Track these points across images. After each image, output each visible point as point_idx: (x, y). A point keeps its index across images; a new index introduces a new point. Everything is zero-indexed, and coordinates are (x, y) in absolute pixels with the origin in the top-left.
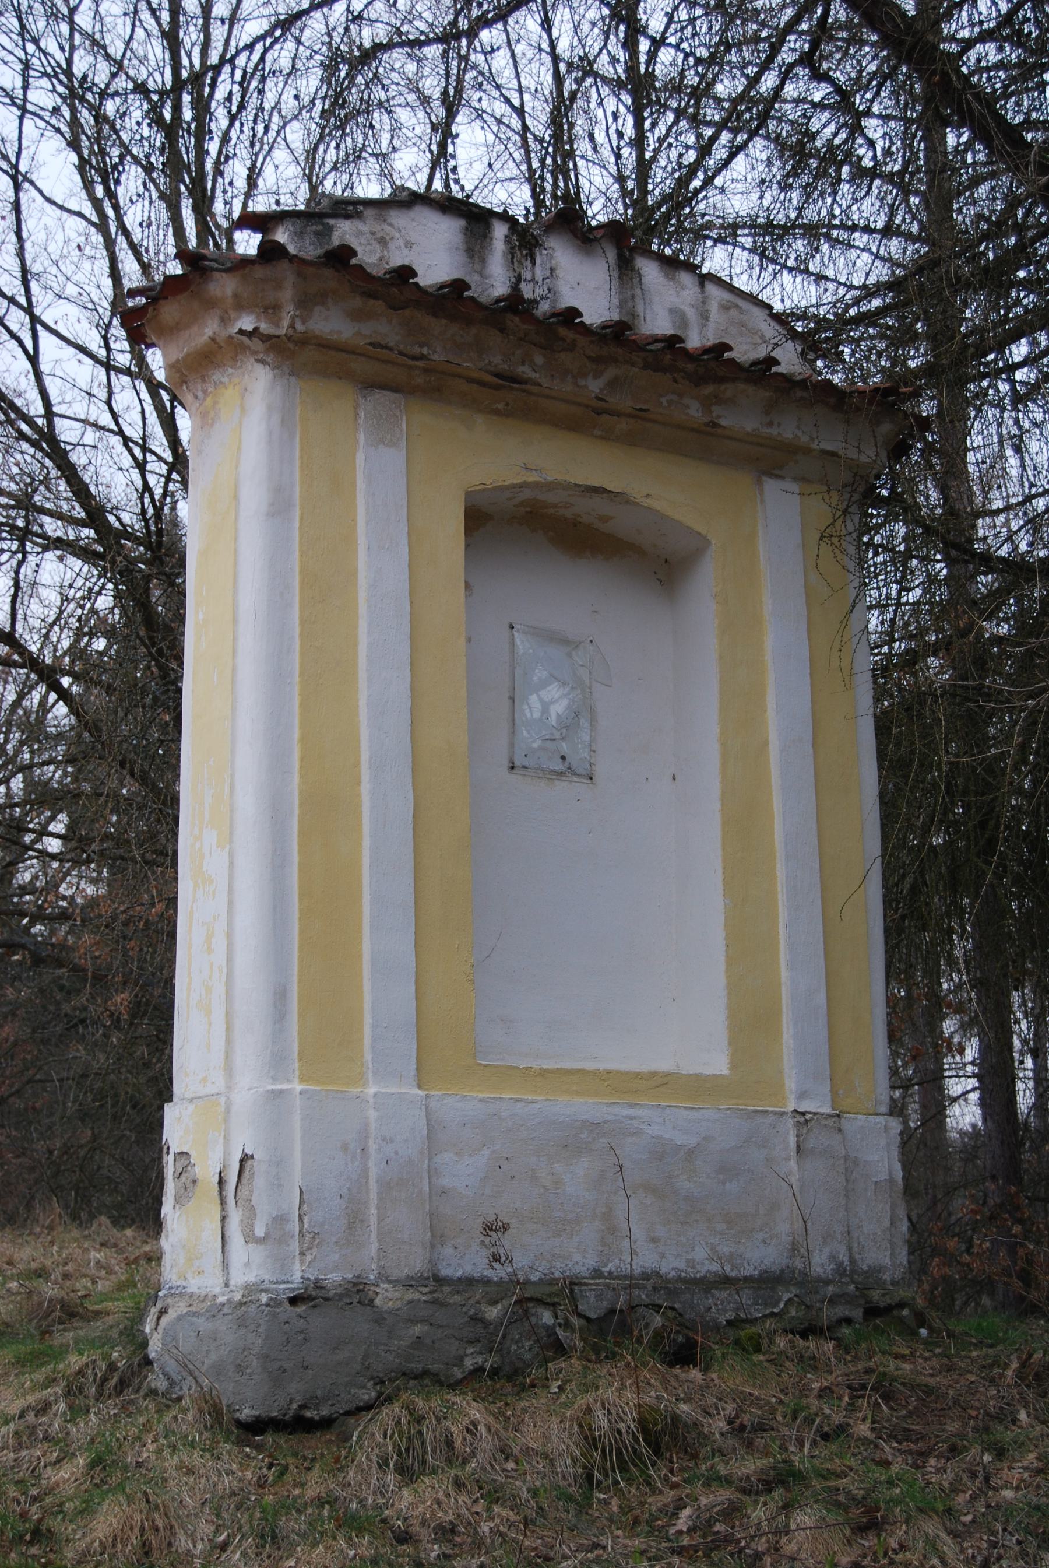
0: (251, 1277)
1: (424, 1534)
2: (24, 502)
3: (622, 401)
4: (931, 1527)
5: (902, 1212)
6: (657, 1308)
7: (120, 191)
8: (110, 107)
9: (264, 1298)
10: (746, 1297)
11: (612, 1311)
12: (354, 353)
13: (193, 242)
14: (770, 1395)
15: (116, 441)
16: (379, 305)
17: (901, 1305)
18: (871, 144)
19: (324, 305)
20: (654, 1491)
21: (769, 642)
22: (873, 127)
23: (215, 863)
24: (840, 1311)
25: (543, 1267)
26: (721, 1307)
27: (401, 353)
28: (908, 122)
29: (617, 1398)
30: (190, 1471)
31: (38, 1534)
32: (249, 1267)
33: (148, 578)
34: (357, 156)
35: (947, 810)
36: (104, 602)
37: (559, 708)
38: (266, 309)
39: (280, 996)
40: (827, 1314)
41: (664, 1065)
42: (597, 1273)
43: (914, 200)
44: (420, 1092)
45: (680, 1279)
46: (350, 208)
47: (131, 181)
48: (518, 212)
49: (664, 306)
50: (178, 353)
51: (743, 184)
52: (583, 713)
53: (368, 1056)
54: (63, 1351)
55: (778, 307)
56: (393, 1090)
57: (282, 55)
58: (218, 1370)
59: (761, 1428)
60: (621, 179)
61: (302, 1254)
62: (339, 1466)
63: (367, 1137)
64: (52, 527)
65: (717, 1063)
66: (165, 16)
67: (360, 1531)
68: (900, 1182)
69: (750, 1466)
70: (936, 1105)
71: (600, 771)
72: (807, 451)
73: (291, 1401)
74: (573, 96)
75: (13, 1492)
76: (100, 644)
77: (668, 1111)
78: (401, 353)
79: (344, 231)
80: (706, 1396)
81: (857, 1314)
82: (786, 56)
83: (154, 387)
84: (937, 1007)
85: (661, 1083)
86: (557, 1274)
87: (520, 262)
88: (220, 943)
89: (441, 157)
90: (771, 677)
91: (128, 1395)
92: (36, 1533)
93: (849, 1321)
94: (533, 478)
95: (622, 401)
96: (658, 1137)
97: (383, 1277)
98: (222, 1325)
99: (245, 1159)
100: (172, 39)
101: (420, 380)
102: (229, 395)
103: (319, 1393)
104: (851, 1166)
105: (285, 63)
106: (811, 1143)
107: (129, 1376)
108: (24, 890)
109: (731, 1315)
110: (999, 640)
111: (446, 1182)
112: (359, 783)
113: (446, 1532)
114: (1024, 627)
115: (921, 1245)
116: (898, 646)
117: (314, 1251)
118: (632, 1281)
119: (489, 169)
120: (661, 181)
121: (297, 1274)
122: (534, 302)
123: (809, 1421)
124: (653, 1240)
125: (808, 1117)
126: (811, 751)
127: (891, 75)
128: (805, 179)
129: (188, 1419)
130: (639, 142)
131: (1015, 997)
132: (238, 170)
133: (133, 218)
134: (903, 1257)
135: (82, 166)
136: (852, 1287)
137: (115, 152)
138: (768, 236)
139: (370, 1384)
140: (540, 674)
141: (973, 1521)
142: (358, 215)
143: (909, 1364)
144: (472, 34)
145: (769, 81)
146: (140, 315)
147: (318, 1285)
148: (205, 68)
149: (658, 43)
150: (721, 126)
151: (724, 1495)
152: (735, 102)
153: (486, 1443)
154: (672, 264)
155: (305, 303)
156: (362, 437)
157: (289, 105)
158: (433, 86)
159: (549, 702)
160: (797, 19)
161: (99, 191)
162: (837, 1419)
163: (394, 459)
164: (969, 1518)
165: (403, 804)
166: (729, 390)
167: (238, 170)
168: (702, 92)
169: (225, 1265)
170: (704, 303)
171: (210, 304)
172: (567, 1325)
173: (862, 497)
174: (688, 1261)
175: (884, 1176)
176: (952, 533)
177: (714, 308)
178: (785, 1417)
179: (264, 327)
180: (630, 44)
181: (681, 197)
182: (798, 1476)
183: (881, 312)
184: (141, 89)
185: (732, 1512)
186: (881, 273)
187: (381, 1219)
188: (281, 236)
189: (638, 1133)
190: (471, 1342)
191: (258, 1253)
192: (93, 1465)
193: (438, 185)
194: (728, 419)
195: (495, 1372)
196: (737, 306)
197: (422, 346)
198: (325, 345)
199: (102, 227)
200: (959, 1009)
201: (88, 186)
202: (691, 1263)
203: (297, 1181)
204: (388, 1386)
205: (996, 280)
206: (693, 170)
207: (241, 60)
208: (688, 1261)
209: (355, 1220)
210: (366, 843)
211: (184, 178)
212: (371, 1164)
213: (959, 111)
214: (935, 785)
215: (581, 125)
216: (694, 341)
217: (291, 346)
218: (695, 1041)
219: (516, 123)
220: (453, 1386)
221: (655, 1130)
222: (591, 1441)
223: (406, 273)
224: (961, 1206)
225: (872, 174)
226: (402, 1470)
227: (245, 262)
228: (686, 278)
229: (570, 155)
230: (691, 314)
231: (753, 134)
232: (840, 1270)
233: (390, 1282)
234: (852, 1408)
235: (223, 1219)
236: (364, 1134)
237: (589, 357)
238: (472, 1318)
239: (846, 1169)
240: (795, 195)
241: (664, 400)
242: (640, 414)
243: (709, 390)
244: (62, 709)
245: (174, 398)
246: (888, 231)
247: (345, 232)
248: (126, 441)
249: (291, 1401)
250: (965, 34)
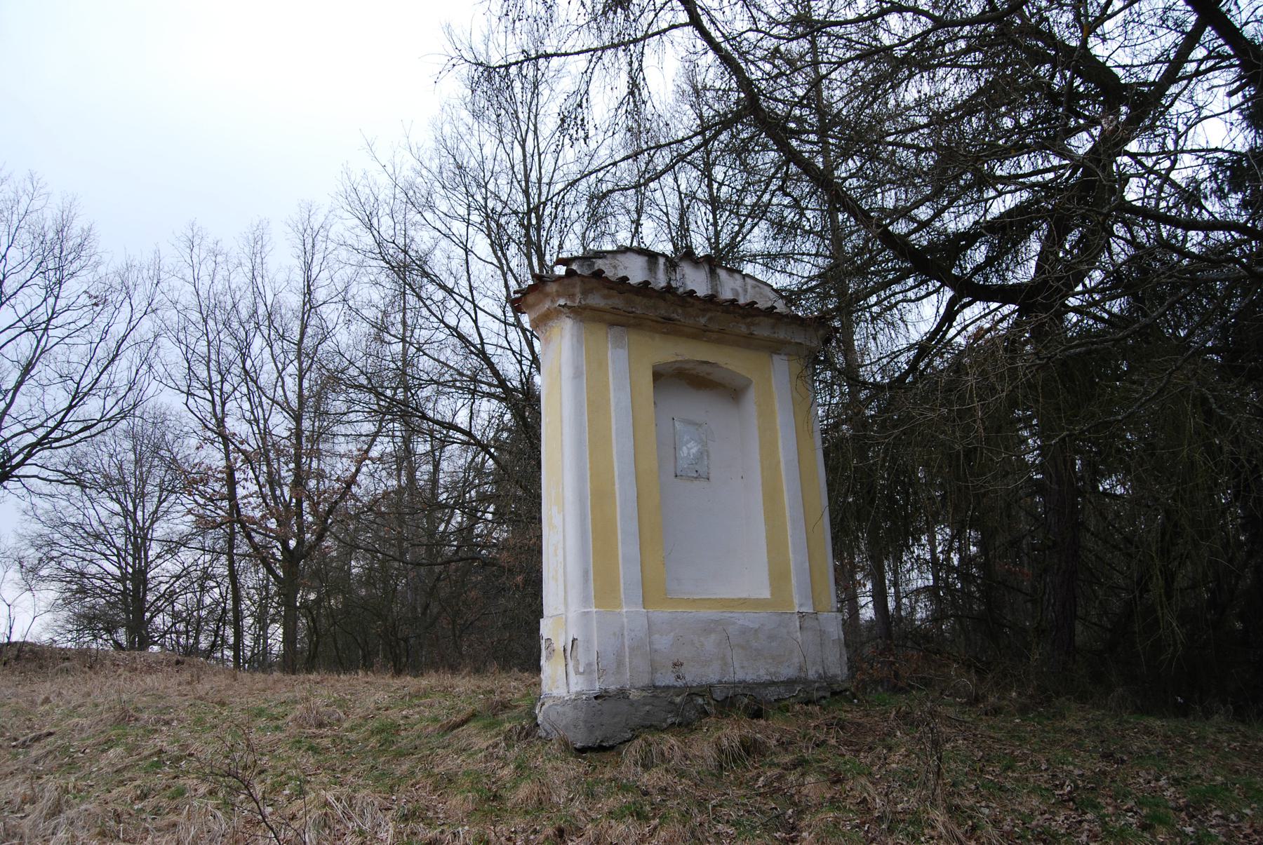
0: (578, 689)
1: (654, 792)
2: (474, 379)
3: (715, 327)
4: (863, 780)
5: (844, 652)
6: (745, 695)
7: (508, 253)
8: (503, 221)
10: (782, 689)
13: (537, 271)
14: (794, 729)
15: (509, 352)
16: (614, 293)
17: (846, 690)
18: (808, 220)
19: (596, 294)
20: (748, 770)
21: (778, 420)
22: (809, 214)
23: (557, 520)
24: (821, 693)
25: (698, 680)
26: (771, 694)
28: (822, 211)
29: (731, 732)
30: (557, 769)
31: (496, 797)
32: (577, 684)
33: (524, 407)
34: (603, 233)
35: (854, 486)
36: (508, 417)
37: (694, 450)
39: (586, 573)
40: (816, 695)
41: (744, 595)
42: (720, 682)
43: (827, 242)
46: (601, 254)
47: (513, 250)
48: (668, 253)
49: (729, 288)
50: (534, 315)
51: (758, 239)
52: (703, 454)
54: (503, 722)
55: (775, 287)
57: (570, 197)
58: (566, 728)
59: (791, 743)
60: (709, 239)
62: (618, 765)
64: (485, 388)
65: (766, 594)
66: (523, 184)
67: (628, 791)
69: (787, 759)
70: (855, 609)
72: (790, 343)
74: (688, 207)
75: (485, 780)
76: (505, 435)
79: (600, 264)
80: (767, 731)
81: (828, 694)
82: (772, 187)
83: (524, 330)
84: (854, 568)
85: (744, 602)
88: (560, 552)
89: (636, 233)
90: (780, 435)
91: (530, 739)
92: (495, 796)
93: (824, 698)
95: (715, 327)
97: (632, 687)
98: (567, 709)
100: (526, 193)
101: (632, 321)
102: (556, 331)
105: (572, 200)
106: (805, 625)
107: (529, 732)
108: (478, 536)
110: (872, 416)
111: (656, 647)
113: (663, 790)
114: (881, 411)
115: (853, 665)
116: (831, 421)
118: (735, 685)
119: (655, 237)
120: (725, 239)
122: (677, 288)
123: (810, 739)
127: (814, 193)
128: (782, 235)
129: (555, 747)
130: (715, 224)
131: (886, 563)
132: (555, 242)
133: (513, 265)
134: (846, 670)
135: (492, 244)
137: (505, 238)
138: (769, 259)
140: (686, 438)
142: (604, 257)
143: (850, 714)
144: (646, 184)
145: (766, 197)
146: (517, 303)
147: (606, 691)
148: (540, 203)
149: (721, 184)
150: (748, 216)
151: (777, 771)
152: (753, 206)
153: (678, 753)
154: (732, 271)
155: (585, 293)
157: (574, 215)
158: (632, 206)
159: (690, 449)
160: (776, 172)
161: (500, 254)
162: (822, 738)
163: (623, 354)
166: (757, 320)
167: (555, 242)
168: (739, 204)
169: (568, 684)
171: (547, 295)
172: (709, 704)
173: (813, 360)
176: (850, 375)
177: (749, 288)
179: (569, 303)
180: (710, 186)
181: (733, 245)
182: (807, 762)
183: (816, 286)
184: (516, 213)
185: (780, 778)
186: (815, 271)
188: (574, 267)
189: (734, 623)
191: (581, 679)
192: (517, 768)
193: (635, 244)
194: (757, 332)
195: (680, 724)
198: (593, 309)
199: (501, 268)
200: (863, 569)
201: (495, 252)
204: (637, 731)
205: (862, 272)
206: (737, 234)
207: (555, 199)
209: (620, 664)
210: (618, 509)
211: (533, 247)
213: (843, 205)
214: (848, 477)
215: (691, 219)
216: (742, 301)
218: (753, 583)
219: (665, 219)
220: (663, 731)
221: (740, 622)
222: (721, 751)
223: (625, 279)
224: (868, 650)
225: (810, 232)
226: (643, 766)
227: (560, 277)
228: (737, 276)
229: (688, 230)
230: (740, 290)
231: (761, 219)
232: (820, 676)
234: (828, 733)
236: (623, 627)
240: (779, 242)
242: (721, 331)
243: (749, 320)
244: (491, 462)
245: (532, 334)
246: (817, 255)
248: (514, 352)
250: (844, 175)
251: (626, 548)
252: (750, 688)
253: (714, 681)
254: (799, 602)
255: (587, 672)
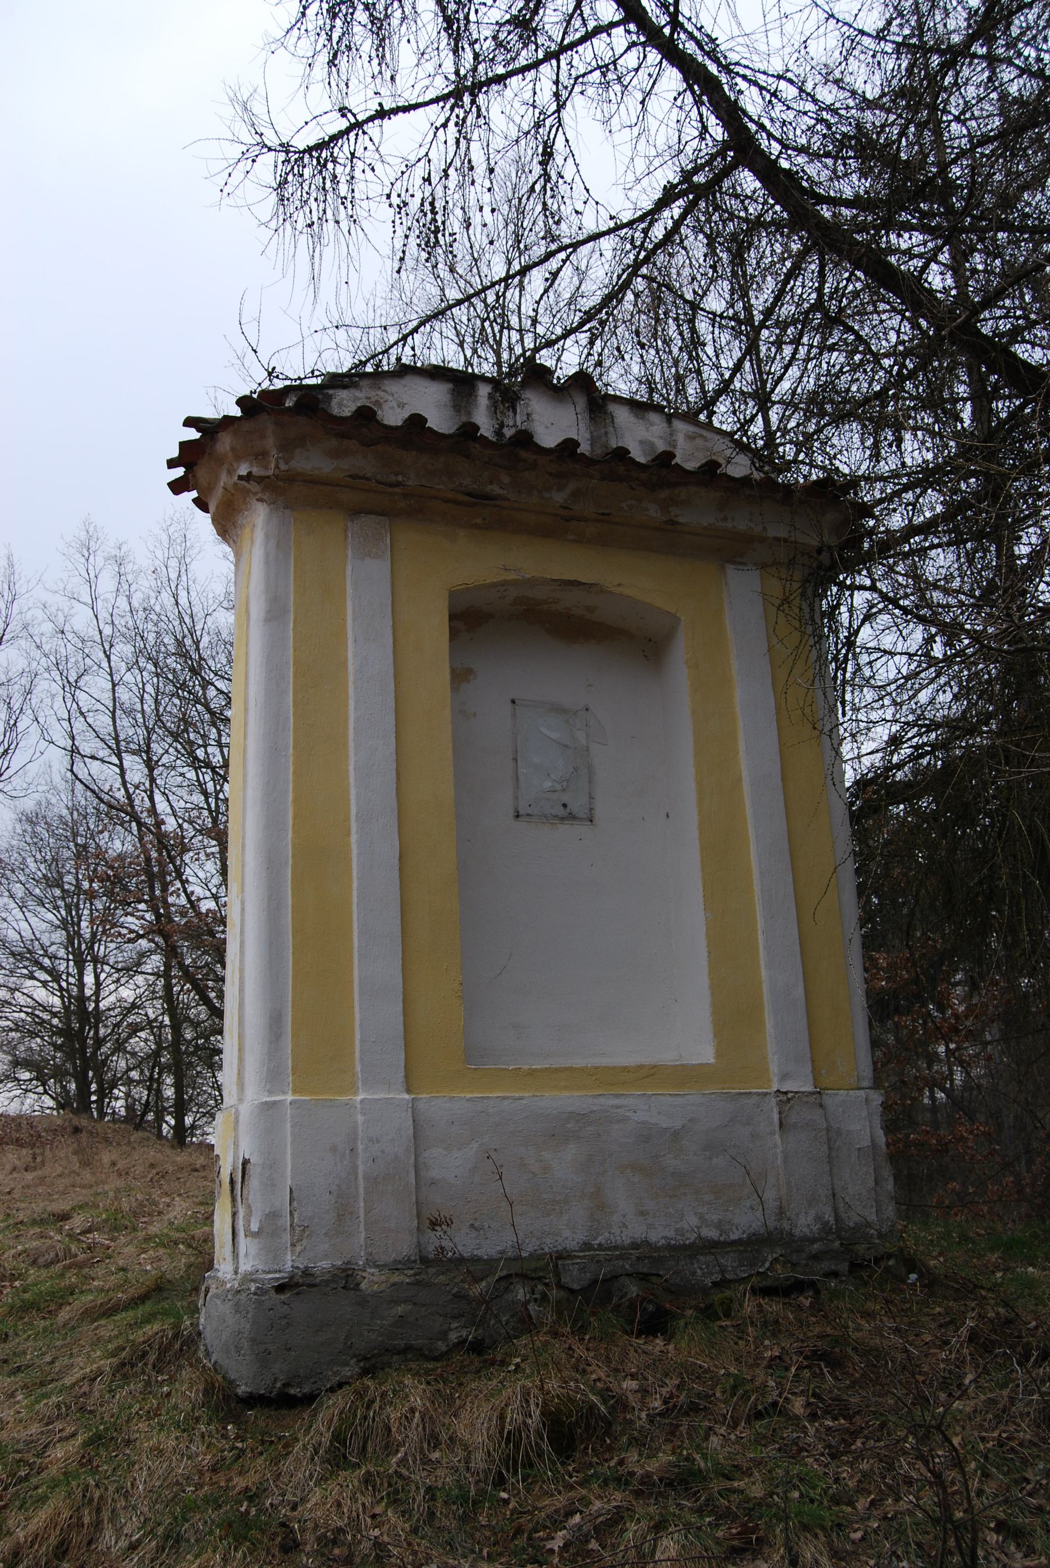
9: (253, 1287)
10: (728, 1261)
11: (596, 1281)
12: (338, 485)
24: (826, 1265)
26: (702, 1271)
27: (378, 482)
38: (256, 456)
39: (275, 1021)
42: (587, 1246)
44: (407, 1096)
45: (669, 1247)
53: (358, 1068)
56: (382, 1096)
61: (293, 1245)
63: (355, 1139)
65: (705, 1053)
68: (884, 1147)
71: (599, 813)
73: (276, 1380)
77: (653, 1098)
78: (378, 482)
81: (844, 1267)
85: (649, 1074)
86: (547, 1250)
87: (502, 413)
90: (740, 724)
93: (835, 1274)
94: (512, 576)
96: (643, 1122)
99: (246, 1162)
103: (301, 1372)
104: (832, 1139)
109: (717, 1277)
111: (435, 1173)
112: (349, 835)
117: (304, 1242)
118: (622, 1251)
121: (289, 1262)
124: (642, 1213)
125: (790, 1095)
126: (780, 784)
136: (837, 1244)
139: (353, 1362)
141: (863, 1539)
147: (306, 1272)
155: (287, 447)
156: (350, 553)
163: (379, 569)
164: (858, 1535)
165: (389, 849)
170: (671, 435)
171: (220, 461)
174: (677, 1230)
175: (866, 1143)
178: (724, 1392)
179: (256, 471)
187: (367, 1212)
190: (454, 1318)
196: (702, 436)
197: (396, 475)
198: (311, 481)
202: (680, 1232)
203: (289, 1182)
208: (677, 1230)
209: (344, 1211)
210: (355, 885)
212: (359, 1162)
217: (281, 484)
233: (378, 1266)
235: (234, 1214)
236: (356, 1128)
237: (550, 474)
238: (454, 1295)
239: (829, 1140)
241: (624, 505)
243: (664, 494)
247: (342, 399)
249: (276, 1380)
251: (372, 967)
252: (648, 1261)
253: (572, 1245)
254: (782, 1070)
255: (268, 1231)
